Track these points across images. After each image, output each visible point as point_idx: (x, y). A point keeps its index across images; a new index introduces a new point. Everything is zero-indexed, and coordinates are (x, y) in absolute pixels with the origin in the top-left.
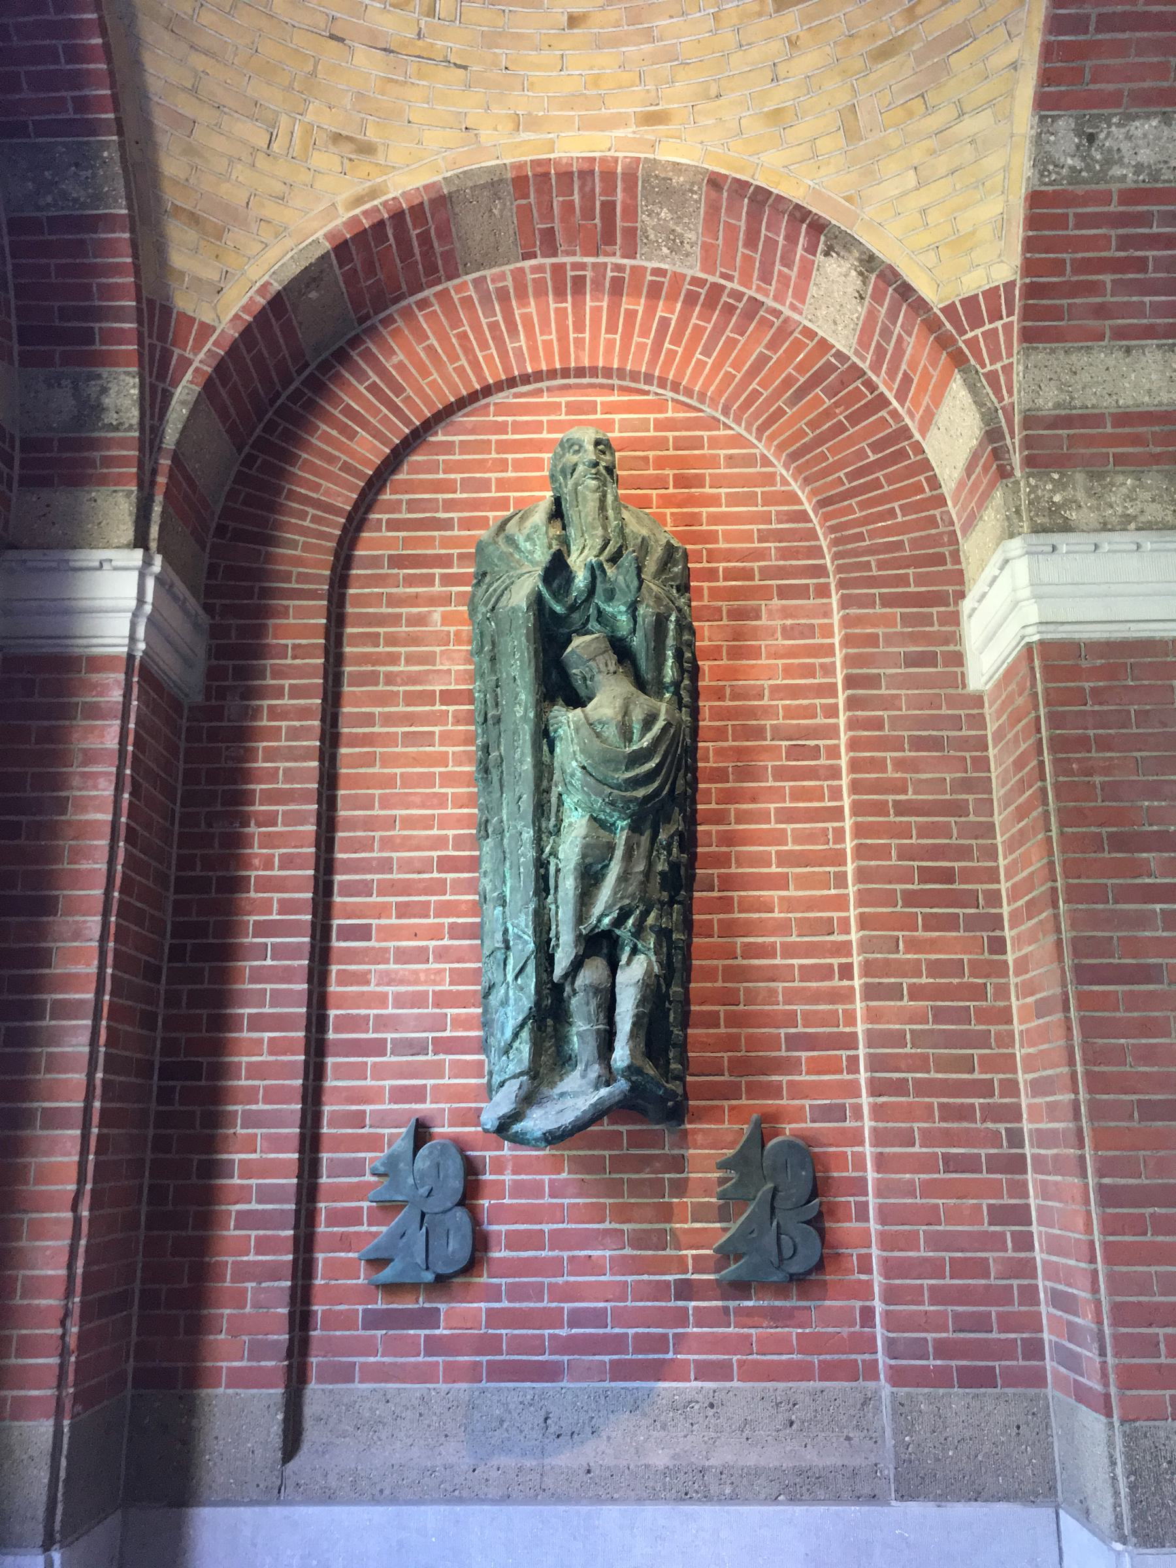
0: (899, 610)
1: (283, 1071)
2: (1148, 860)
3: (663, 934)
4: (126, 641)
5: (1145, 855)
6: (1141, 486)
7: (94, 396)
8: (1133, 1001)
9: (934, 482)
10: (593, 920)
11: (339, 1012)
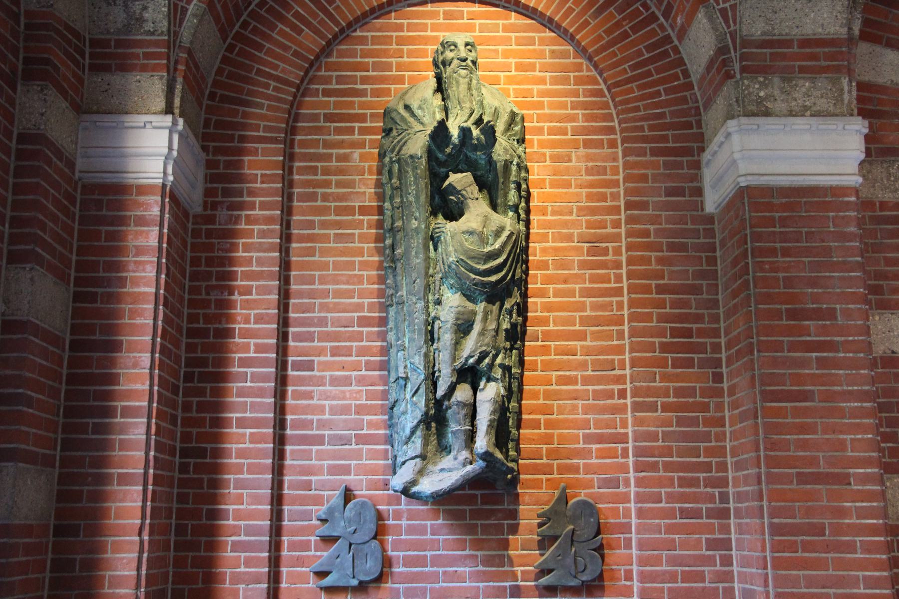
0: (662, 158)
1: (259, 454)
2: (809, 326)
3: (506, 369)
4: (162, 175)
5: (807, 323)
6: (814, 88)
7: (138, 12)
8: (797, 412)
9: (686, 73)
10: (463, 360)
11: (294, 417)
